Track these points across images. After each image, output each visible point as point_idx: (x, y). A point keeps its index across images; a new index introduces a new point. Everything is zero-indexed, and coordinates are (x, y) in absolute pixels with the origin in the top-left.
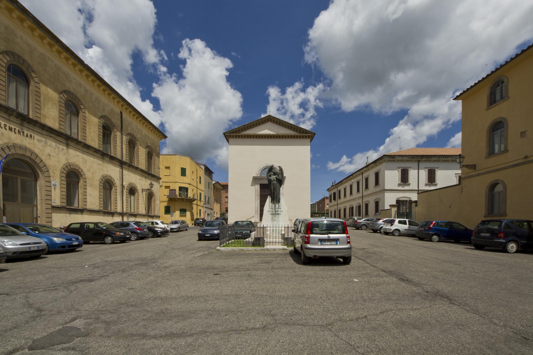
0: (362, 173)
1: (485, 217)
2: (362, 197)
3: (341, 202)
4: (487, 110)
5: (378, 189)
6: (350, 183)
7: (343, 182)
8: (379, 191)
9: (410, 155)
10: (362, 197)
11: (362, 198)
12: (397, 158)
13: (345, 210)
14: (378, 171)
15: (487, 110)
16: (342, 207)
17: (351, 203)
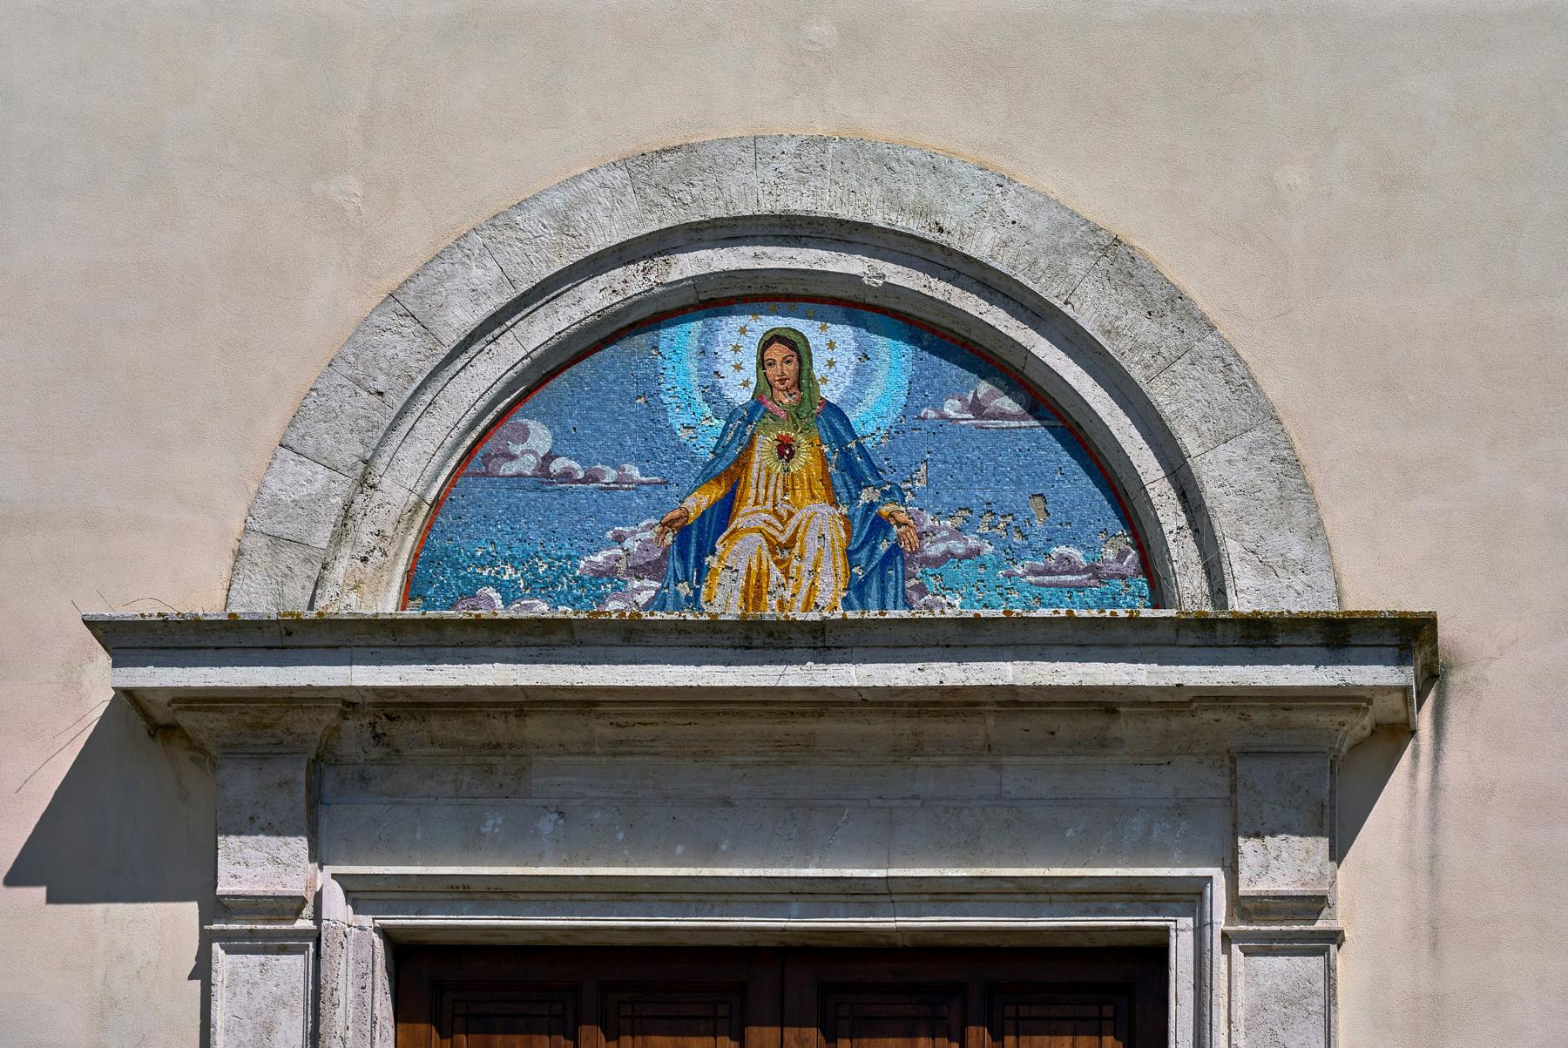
4: (91, 624)
15: (91, 624)
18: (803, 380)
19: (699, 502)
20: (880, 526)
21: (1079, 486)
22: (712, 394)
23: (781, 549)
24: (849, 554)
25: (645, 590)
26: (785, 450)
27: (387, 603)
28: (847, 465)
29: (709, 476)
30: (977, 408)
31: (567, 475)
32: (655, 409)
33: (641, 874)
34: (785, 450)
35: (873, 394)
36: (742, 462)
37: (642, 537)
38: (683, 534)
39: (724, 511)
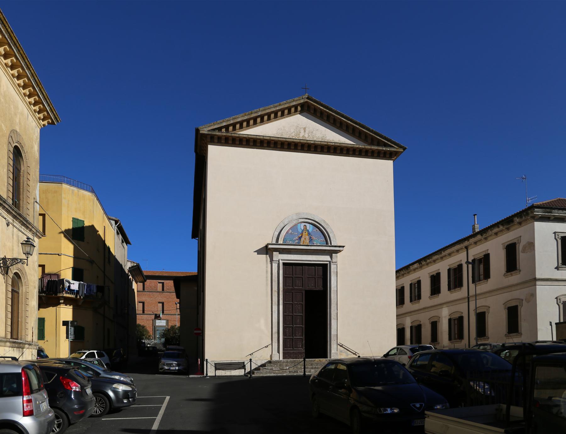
0: (467, 248)
1: (156, 418)
2: (468, 298)
3: (422, 307)
4: (131, 245)
5: (514, 278)
6: (432, 269)
7: (412, 268)
8: (517, 285)
9: (503, 221)
10: (468, 298)
11: (467, 300)
12: (517, 220)
13: (434, 325)
14: (515, 241)
15: (131, 245)
16: (425, 320)
17: (416, 317)
18: (306, 228)
19: (300, 236)
20: (311, 238)
21: (322, 236)
22: (301, 229)
23: (305, 239)
24: (309, 239)
25: (297, 241)
26: (305, 232)
27: (282, 243)
28: (309, 233)
29: (301, 234)
30: (316, 230)
31: (292, 234)
32: (298, 230)
33: (197, 269)
34: (305, 232)
35: (310, 229)
36: (303, 233)
37: (297, 238)
38: (299, 238)
39: (302, 236)
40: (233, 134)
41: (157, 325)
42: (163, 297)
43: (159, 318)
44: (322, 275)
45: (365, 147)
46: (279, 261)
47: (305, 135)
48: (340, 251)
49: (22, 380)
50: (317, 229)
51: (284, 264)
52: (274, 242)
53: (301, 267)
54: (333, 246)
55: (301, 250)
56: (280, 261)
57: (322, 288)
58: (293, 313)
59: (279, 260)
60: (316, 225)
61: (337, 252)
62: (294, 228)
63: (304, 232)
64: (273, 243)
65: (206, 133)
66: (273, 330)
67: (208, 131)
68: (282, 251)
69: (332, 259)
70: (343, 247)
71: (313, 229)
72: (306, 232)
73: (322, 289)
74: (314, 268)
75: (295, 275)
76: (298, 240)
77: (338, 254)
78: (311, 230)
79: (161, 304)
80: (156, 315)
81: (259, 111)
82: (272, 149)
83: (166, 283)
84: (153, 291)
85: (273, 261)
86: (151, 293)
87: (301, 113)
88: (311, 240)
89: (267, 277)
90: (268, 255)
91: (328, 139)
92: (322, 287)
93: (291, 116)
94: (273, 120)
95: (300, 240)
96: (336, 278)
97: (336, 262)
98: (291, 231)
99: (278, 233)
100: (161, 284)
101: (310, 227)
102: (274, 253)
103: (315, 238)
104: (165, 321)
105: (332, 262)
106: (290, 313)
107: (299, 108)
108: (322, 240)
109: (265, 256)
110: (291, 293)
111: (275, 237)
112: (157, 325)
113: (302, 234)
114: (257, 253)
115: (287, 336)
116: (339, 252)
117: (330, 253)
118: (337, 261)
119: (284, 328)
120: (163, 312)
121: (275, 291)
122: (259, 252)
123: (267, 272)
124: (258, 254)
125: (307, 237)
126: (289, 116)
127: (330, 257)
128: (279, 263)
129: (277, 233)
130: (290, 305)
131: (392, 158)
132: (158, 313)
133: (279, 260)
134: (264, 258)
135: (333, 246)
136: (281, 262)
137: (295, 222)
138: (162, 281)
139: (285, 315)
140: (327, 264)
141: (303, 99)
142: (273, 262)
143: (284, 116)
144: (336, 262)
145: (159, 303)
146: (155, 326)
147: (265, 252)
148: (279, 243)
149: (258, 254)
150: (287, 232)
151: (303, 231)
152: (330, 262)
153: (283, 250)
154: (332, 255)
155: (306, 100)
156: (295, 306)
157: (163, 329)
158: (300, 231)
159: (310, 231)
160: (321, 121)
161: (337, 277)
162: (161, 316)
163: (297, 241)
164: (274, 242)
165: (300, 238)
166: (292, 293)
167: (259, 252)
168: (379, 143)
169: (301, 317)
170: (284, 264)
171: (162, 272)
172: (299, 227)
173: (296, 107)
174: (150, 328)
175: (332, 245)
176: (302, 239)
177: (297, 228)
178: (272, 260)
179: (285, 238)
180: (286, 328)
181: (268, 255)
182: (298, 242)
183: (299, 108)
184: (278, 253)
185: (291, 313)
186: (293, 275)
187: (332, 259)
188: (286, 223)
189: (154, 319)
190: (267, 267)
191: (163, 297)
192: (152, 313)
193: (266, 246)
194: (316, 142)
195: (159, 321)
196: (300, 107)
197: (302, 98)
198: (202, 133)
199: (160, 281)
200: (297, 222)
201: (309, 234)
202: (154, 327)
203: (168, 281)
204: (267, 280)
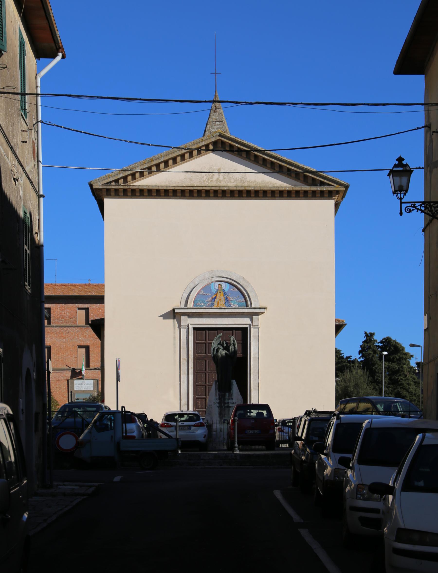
18: (221, 287)
19: (214, 296)
20: (227, 298)
21: (241, 295)
22: (215, 288)
23: (220, 300)
24: (225, 300)
25: (210, 303)
26: (220, 292)
27: (192, 307)
28: (224, 293)
30: (234, 290)
31: (205, 294)
34: (220, 292)
35: (226, 288)
36: (217, 293)
37: (210, 299)
38: (213, 299)
39: (216, 297)
40: (131, 186)
41: (75, 389)
42: (87, 336)
43: (80, 377)
44: (241, 340)
45: (293, 188)
46: (188, 326)
47: (219, 177)
48: (263, 313)
49: (46, 396)
50: (234, 288)
51: (194, 329)
52: (183, 306)
53: (216, 331)
54: (255, 308)
55: (215, 314)
56: (190, 326)
57: (241, 354)
58: (206, 383)
59: (188, 325)
60: (233, 284)
61: (257, 314)
62: (207, 288)
63: (219, 292)
64: (181, 307)
65: (101, 187)
66: (182, 401)
67: (102, 185)
68: (191, 315)
69: (252, 322)
70: (265, 308)
71: (230, 288)
72: (221, 292)
73: (242, 356)
74: (231, 332)
75: (209, 340)
76: (211, 301)
77: (260, 316)
78: (228, 290)
79: (84, 350)
80: (74, 370)
81: (160, 157)
82: (179, 198)
83: (94, 309)
84: (67, 325)
85: (182, 326)
86: (63, 330)
87: (213, 151)
88: (227, 301)
89: (174, 344)
90: (175, 320)
91: (249, 180)
92: (242, 354)
93: (201, 156)
94: (180, 163)
95: (214, 302)
96: (258, 343)
97: (257, 326)
98: (203, 292)
99: (187, 295)
100: (83, 312)
101: (226, 286)
102: (183, 318)
103: (233, 298)
104: (92, 381)
105: (253, 326)
106: (203, 383)
107: (211, 147)
108: (240, 301)
109: (172, 320)
110: (203, 361)
111: (184, 299)
112: (75, 389)
113: (216, 294)
114: (162, 317)
115: (199, 409)
116: (261, 313)
117: (250, 315)
118: (259, 323)
119: (195, 399)
120: (88, 365)
121: (184, 359)
122: (165, 316)
123: (174, 338)
124: (163, 319)
125: (223, 298)
126: (199, 157)
127: (250, 319)
128: (188, 328)
129: (186, 295)
130: (203, 374)
131: (332, 197)
132: (77, 367)
133: (188, 325)
134: (171, 322)
135: (255, 308)
136: (191, 327)
137: (206, 282)
138: (85, 306)
139: (197, 385)
140: (247, 328)
141: (213, 137)
142: (181, 327)
143: (193, 157)
144: (257, 326)
145: (80, 347)
146: (71, 392)
147: (172, 316)
148: (188, 307)
149: (163, 319)
150: (198, 294)
151: (217, 291)
152: (250, 325)
153: (192, 314)
154: (252, 317)
155: (218, 138)
156: (208, 375)
157: (84, 397)
158: (214, 291)
159: (226, 291)
160: (239, 158)
161: (259, 342)
162: (83, 372)
163: (210, 303)
164: (183, 306)
165: (214, 299)
166: (205, 361)
167: (165, 316)
168: (314, 183)
169: (205, 387)
170: (194, 329)
171: (86, 285)
172: (212, 287)
173: (207, 146)
174: (63, 396)
175: (253, 306)
176: (216, 300)
177: (210, 288)
178: (180, 326)
179: (195, 299)
180: (197, 399)
181: (175, 320)
182: (211, 304)
183: (211, 147)
184: (187, 317)
185: (204, 383)
186: (205, 341)
187: (252, 322)
188: (196, 283)
189: (69, 378)
190: (174, 333)
191: (87, 336)
192: (65, 367)
193: (174, 310)
194: (230, 188)
195: (80, 382)
196: (212, 145)
197: (212, 136)
198: (95, 187)
199: (81, 306)
200: (210, 281)
201: (225, 294)
202: (70, 393)
203: (96, 305)
204: (175, 347)
